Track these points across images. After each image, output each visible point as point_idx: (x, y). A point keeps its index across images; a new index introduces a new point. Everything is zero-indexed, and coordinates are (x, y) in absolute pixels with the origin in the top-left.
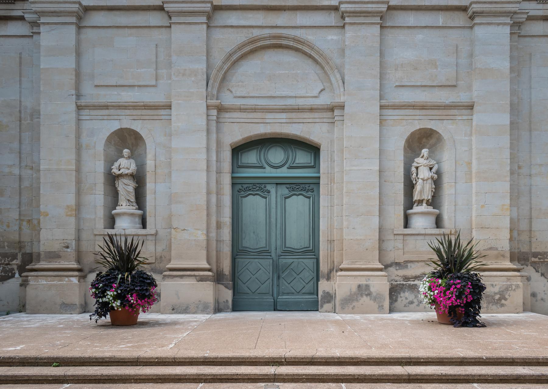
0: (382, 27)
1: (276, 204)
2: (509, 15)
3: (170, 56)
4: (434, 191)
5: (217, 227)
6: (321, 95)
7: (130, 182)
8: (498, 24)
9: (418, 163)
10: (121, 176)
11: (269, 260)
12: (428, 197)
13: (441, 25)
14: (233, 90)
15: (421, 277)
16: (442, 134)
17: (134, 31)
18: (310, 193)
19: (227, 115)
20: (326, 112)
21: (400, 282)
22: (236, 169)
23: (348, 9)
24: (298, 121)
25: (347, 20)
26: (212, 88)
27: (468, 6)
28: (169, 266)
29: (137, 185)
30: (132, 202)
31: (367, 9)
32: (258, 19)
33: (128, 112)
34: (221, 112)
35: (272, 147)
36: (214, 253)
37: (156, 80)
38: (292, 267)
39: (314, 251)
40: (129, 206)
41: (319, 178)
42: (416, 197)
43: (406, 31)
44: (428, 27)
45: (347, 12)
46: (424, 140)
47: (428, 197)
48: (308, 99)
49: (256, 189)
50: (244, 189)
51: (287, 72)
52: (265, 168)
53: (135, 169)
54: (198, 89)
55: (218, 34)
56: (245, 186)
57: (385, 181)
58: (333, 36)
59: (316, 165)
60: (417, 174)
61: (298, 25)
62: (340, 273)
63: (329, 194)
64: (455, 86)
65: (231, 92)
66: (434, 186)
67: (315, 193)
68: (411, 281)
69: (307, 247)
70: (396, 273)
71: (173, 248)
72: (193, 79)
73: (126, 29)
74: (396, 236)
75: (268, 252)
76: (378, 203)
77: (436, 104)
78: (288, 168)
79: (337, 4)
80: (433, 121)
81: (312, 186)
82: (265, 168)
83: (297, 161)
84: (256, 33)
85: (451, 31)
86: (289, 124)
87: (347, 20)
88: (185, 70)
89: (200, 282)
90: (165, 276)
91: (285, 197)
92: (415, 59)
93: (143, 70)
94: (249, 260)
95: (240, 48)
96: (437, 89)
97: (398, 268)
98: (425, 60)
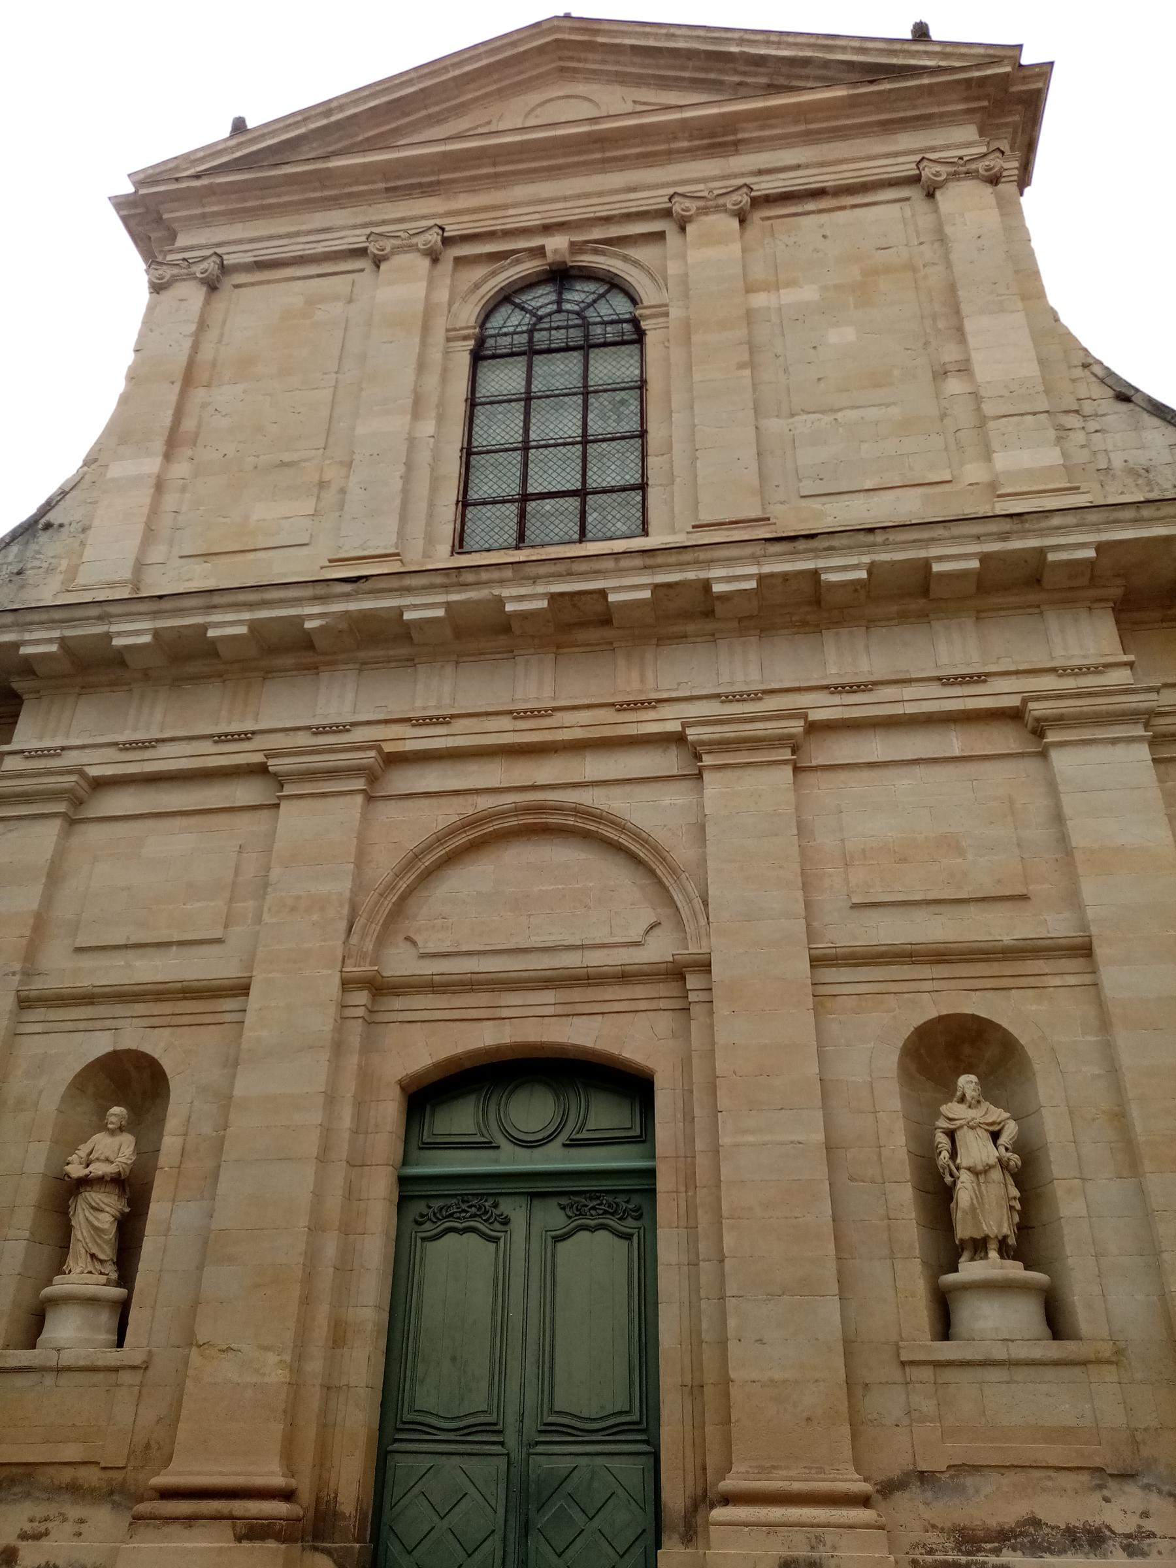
0: (797, 769)
1: (528, 1260)
2: (1138, 719)
3: (268, 869)
4: (1018, 1207)
5: (334, 1341)
6: (649, 939)
7: (106, 1200)
8: (1114, 741)
9: (951, 1120)
10: (85, 1182)
11: (495, 1458)
12: (1000, 1226)
13: (957, 753)
14: (418, 939)
15: (1021, 1534)
16: (1011, 1029)
17: (193, 821)
18: (630, 1222)
19: (398, 1003)
20: (665, 981)
21: (946, 1553)
22: (415, 1154)
23: (705, 737)
24: (588, 1008)
25: (708, 760)
26: (363, 936)
27: (1021, 708)
28: (163, 1480)
29: (127, 1210)
30: (102, 1262)
31: (45, 786)
32: (493, 774)
33: (140, 1008)
34: (382, 995)
35: (516, 1088)
36: (309, 1434)
37: (226, 927)
38: (568, 1487)
39: (644, 1426)
40: (90, 1272)
41: (651, 1173)
42: (963, 1231)
43: (866, 774)
44: (922, 759)
45: (702, 743)
46: (967, 1050)
47: (1000, 1226)
48: (616, 950)
49: (468, 1214)
50: (435, 1214)
51: (560, 887)
52: (498, 1147)
53: (130, 1162)
54: (325, 941)
55: (389, 813)
56: (436, 1204)
57: (852, 1179)
58: (676, 798)
59: (645, 1136)
60: (954, 1155)
61: (586, 780)
62: (719, 1513)
63: (683, 1223)
64: (1024, 898)
65: (414, 943)
66: (1014, 1192)
67: (646, 1220)
68: (985, 1550)
69: (621, 1413)
70: (926, 1516)
71: (184, 1413)
72: (315, 917)
73: (179, 818)
74: (907, 1369)
75: (493, 1428)
76: (831, 1248)
77: (975, 945)
78: (565, 1145)
79: (680, 729)
80: (977, 993)
81: (636, 1200)
82: (498, 1147)
83: (591, 1125)
84: (485, 803)
85: (987, 766)
86: (564, 1018)
87: (708, 760)
88: (299, 897)
89: (246, 1544)
90: (137, 1518)
91: (553, 1238)
92: (899, 836)
93: (199, 904)
94: (427, 1462)
95: (441, 838)
96: (972, 908)
97: (929, 1494)
98: (926, 838)
